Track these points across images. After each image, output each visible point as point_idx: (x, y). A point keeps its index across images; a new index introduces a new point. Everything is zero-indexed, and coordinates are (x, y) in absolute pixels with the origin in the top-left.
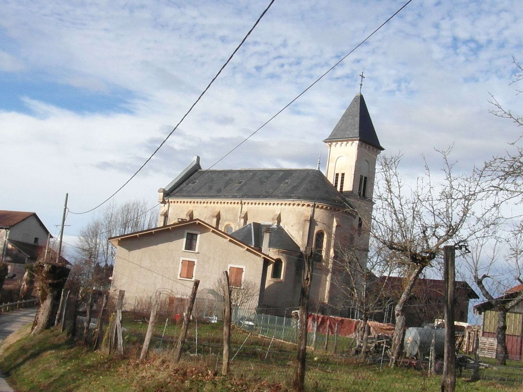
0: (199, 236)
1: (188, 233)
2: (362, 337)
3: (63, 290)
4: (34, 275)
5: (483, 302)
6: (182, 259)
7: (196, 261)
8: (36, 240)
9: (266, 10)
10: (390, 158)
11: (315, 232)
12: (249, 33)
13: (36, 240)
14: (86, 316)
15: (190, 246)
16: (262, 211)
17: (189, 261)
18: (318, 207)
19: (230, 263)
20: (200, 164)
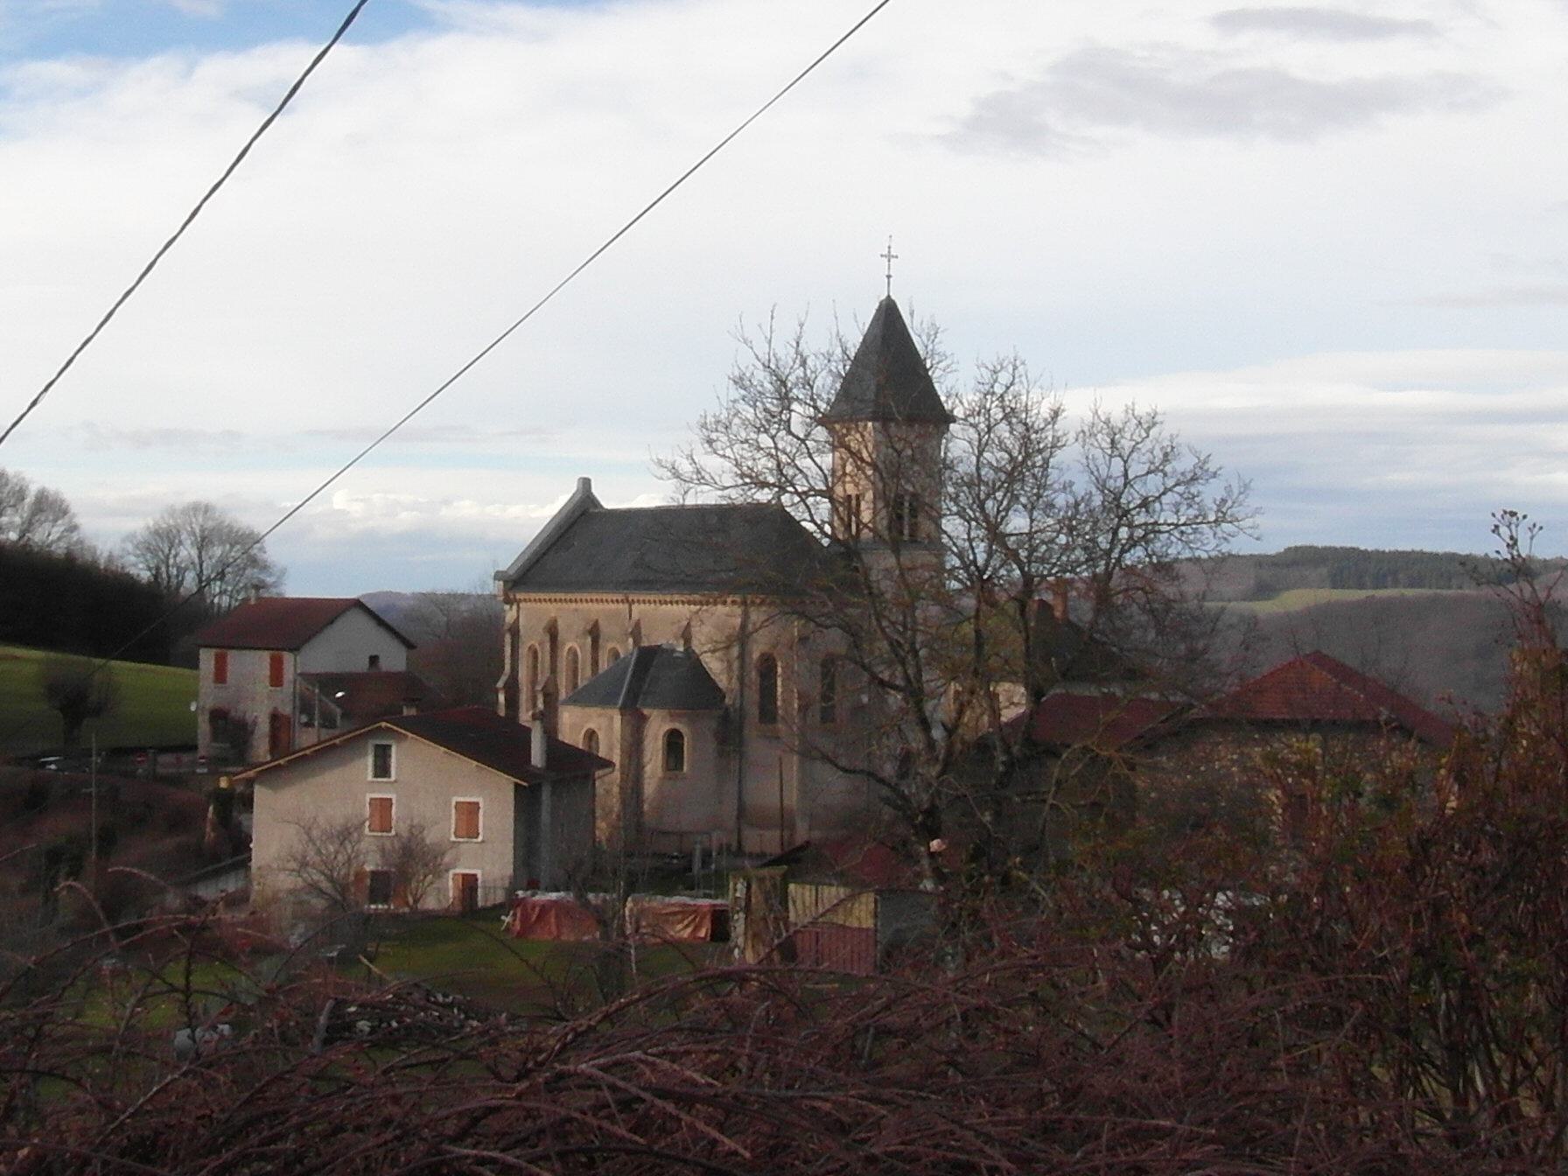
0: (394, 749)
1: (377, 746)
2: (784, 452)
3: (562, 894)
4: (214, 1079)
5: (922, 353)
6: (369, 796)
7: (393, 797)
8: (374, 660)
9: (98, 329)
10: (736, 393)
11: (756, 656)
12: (46, 389)
13: (374, 660)
14: (376, 776)
15: (382, 769)
16: (664, 617)
17: (164, 660)
18: (753, 603)
19: (456, 794)
20: (594, 490)
